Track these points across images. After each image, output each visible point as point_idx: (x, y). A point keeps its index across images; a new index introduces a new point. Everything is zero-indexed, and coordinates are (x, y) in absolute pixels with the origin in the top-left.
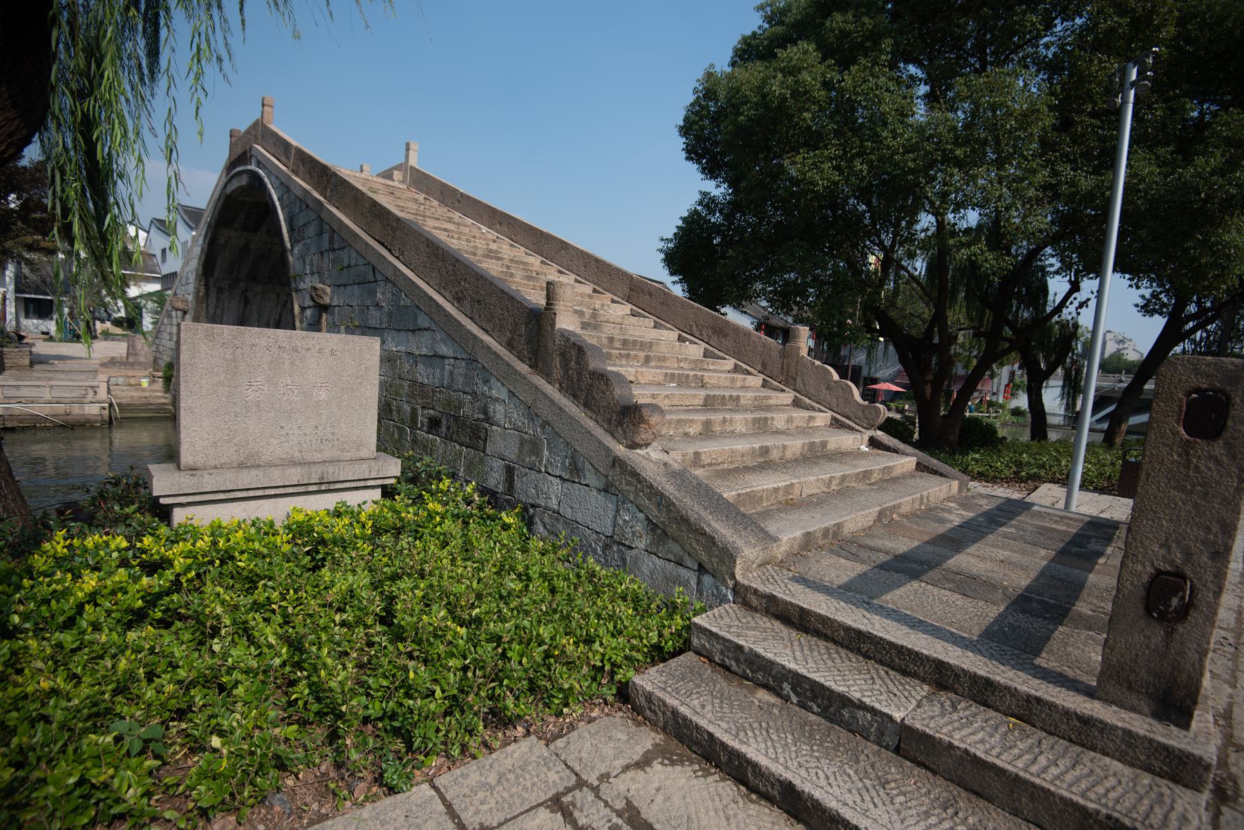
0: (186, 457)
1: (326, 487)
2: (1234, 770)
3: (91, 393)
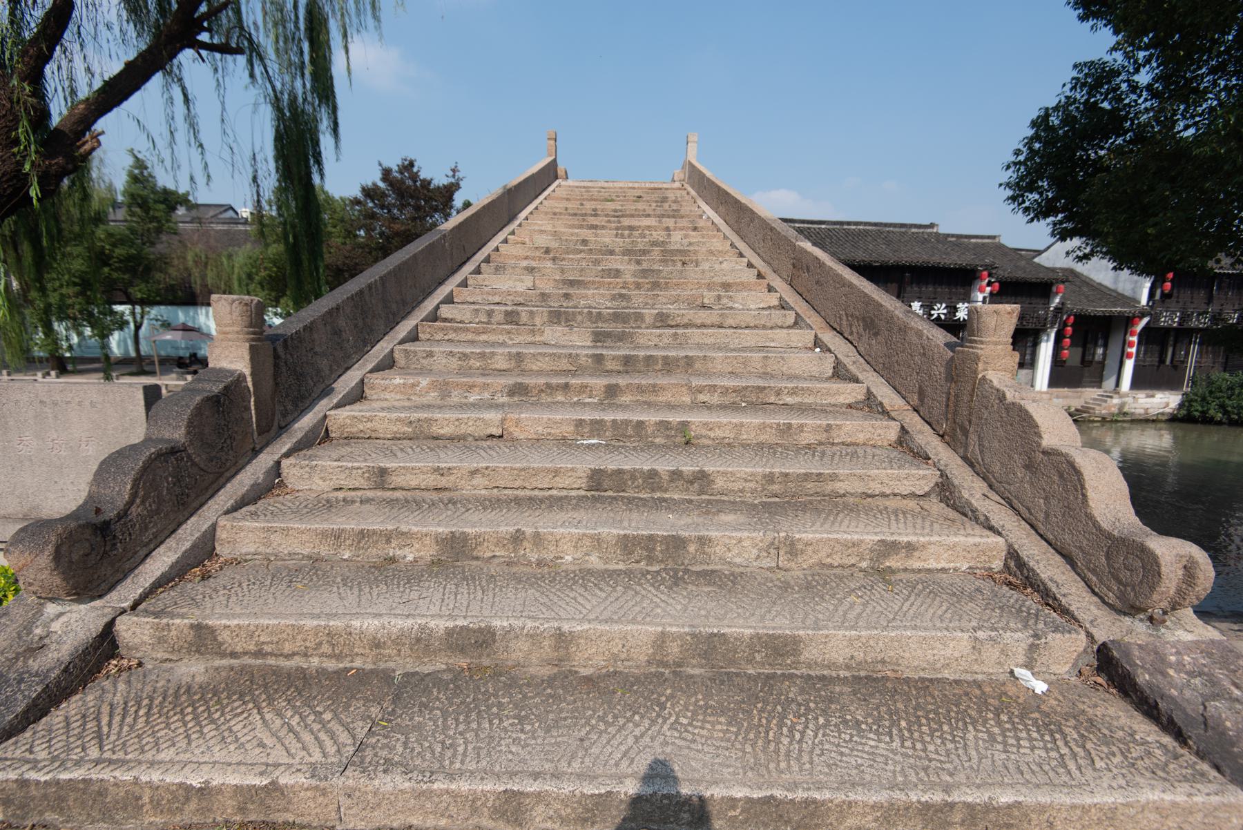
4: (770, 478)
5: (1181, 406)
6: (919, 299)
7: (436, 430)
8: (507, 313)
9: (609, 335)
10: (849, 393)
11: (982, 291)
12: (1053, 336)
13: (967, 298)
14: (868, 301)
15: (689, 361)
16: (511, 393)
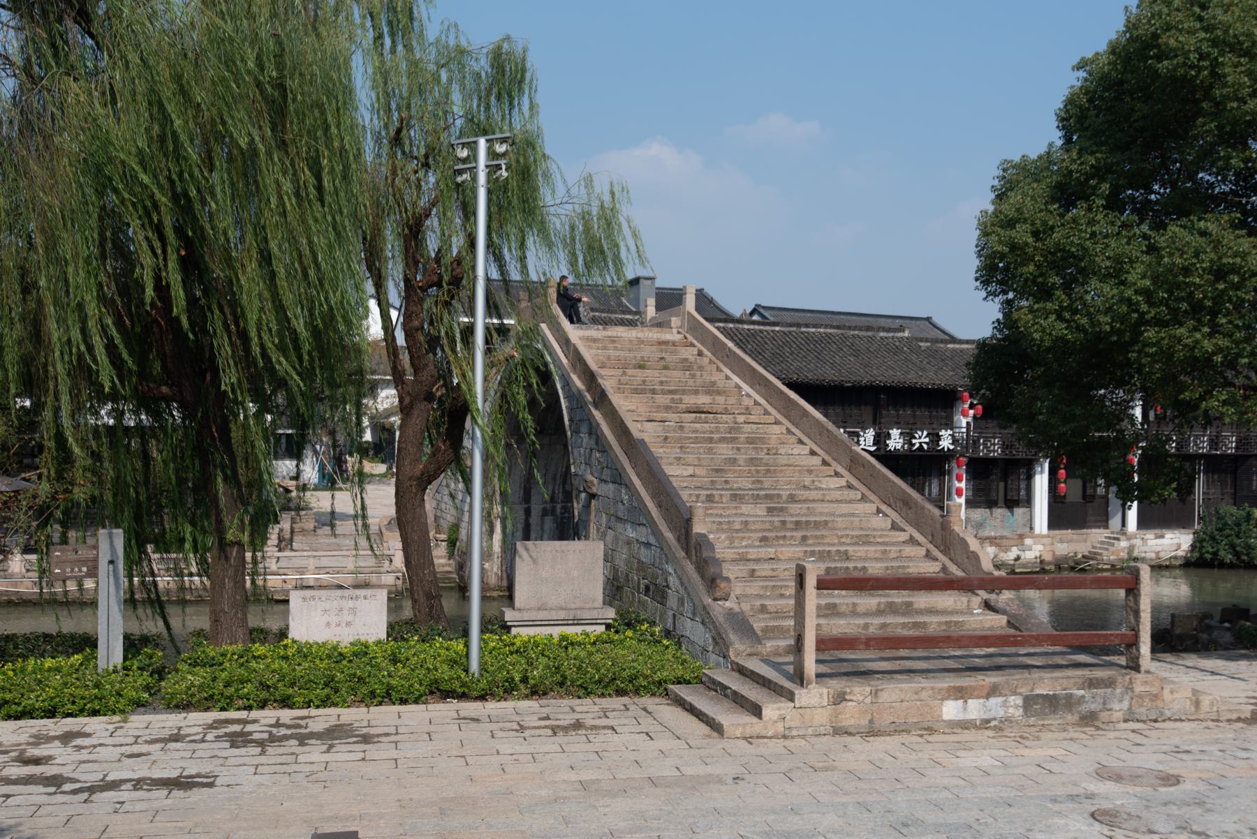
0: (517, 604)
1: (577, 622)
2: (813, 696)
3: (387, 563)
4: (887, 568)
5: (1193, 546)
6: (897, 425)
7: (750, 557)
8: (708, 496)
9: (775, 508)
10: (903, 536)
11: (965, 414)
12: (1046, 466)
13: (949, 424)
14: (905, 492)
15: (826, 522)
16: (761, 541)
